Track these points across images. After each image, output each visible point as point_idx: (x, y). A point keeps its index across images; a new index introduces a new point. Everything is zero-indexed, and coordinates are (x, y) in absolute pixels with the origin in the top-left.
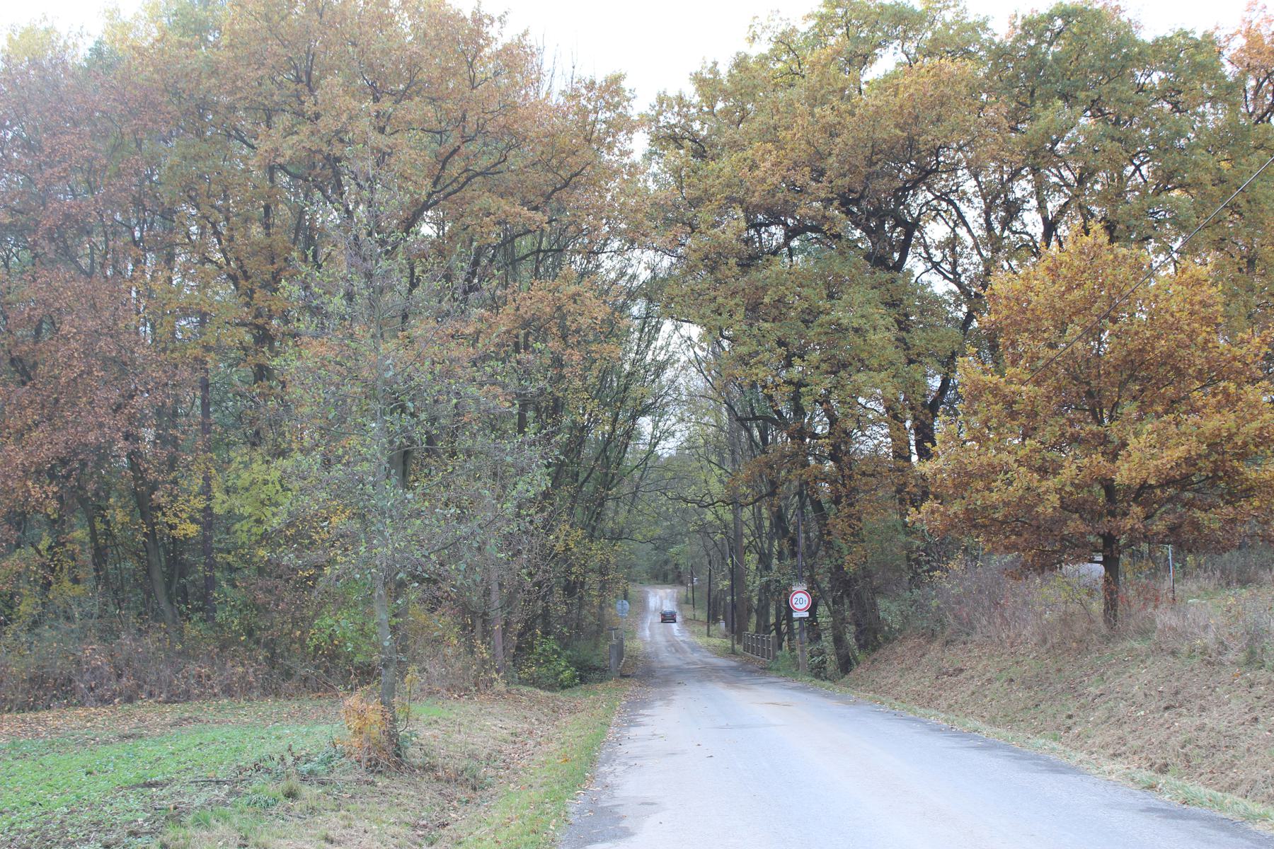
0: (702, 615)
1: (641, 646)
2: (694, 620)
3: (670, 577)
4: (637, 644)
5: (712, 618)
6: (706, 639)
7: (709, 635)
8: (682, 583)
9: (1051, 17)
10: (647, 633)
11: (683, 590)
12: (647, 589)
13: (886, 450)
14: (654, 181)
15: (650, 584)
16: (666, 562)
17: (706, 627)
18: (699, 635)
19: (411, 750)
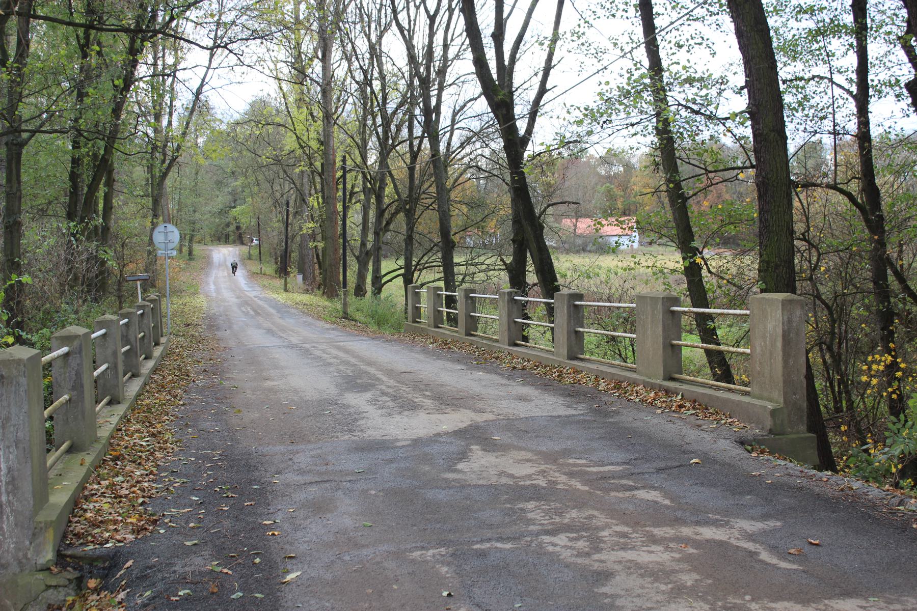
0: (270, 269)
1: (205, 305)
2: (262, 274)
3: (231, 238)
4: (200, 301)
5: (283, 271)
6: (285, 295)
7: (286, 290)
8: (242, 243)
9: (695, 453)
10: (212, 287)
11: (245, 249)
12: (210, 248)
13: (83, 29)
14: (116, 55)
15: (213, 245)
16: (228, 225)
17: (875, 132)
18: (275, 290)
19: (235, 326)
